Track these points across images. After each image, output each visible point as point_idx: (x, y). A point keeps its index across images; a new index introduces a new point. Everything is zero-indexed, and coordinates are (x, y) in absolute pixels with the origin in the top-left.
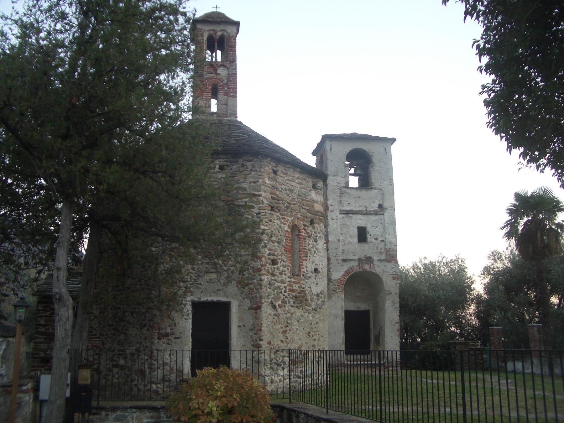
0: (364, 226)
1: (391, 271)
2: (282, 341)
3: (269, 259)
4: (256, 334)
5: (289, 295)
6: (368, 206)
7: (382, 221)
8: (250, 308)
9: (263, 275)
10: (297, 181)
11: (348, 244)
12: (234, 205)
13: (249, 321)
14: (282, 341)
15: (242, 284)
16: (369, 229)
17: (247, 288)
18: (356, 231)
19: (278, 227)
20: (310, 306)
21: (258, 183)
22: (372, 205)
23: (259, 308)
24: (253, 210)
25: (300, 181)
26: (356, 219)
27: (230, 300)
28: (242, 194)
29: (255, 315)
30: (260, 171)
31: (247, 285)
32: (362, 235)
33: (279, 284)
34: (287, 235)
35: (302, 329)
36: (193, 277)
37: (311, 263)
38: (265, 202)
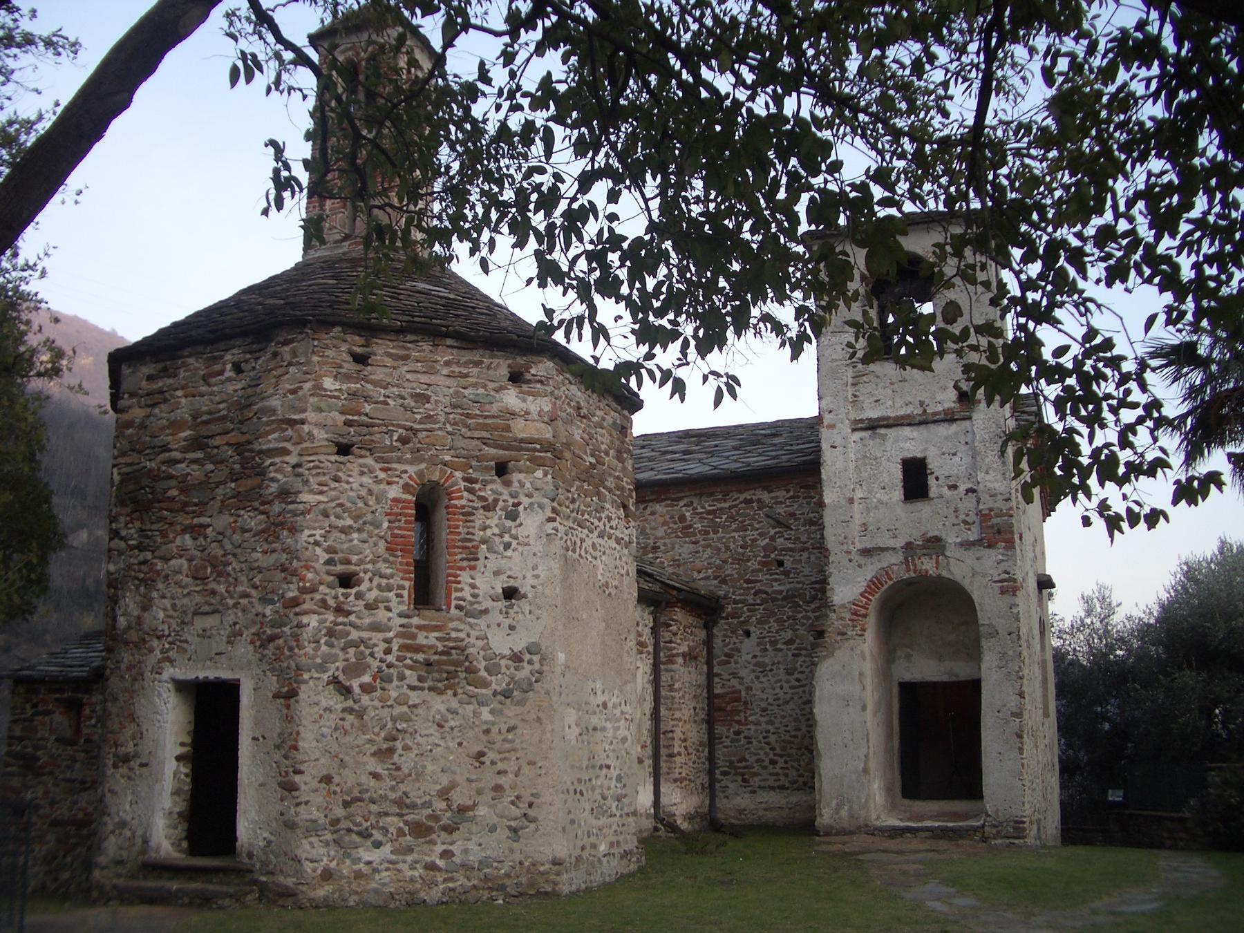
0: (919, 455)
1: (995, 573)
2: (376, 776)
3: (328, 573)
4: (286, 757)
5: (399, 659)
6: (927, 401)
7: (969, 439)
8: (277, 696)
9: (306, 613)
10: (445, 371)
11: (876, 507)
12: (252, 451)
13: (274, 727)
14: (376, 776)
15: (263, 641)
16: (933, 464)
17: (271, 646)
18: (897, 472)
19: (363, 493)
20: (485, 684)
21: (300, 393)
22: (940, 397)
23: (293, 694)
24: (287, 459)
25: (457, 370)
26: (897, 440)
27: (225, 675)
28: (267, 424)
29: (285, 711)
30: (308, 362)
31: (272, 639)
32: (915, 479)
33: (365, 635)
34: (396, 510)
35: (453, 745)
36: (174, 626)
37: (489, 574)
38: (320, 434)
